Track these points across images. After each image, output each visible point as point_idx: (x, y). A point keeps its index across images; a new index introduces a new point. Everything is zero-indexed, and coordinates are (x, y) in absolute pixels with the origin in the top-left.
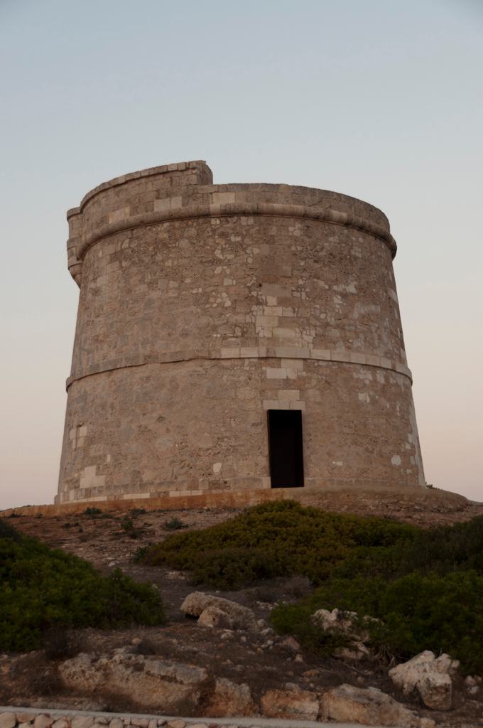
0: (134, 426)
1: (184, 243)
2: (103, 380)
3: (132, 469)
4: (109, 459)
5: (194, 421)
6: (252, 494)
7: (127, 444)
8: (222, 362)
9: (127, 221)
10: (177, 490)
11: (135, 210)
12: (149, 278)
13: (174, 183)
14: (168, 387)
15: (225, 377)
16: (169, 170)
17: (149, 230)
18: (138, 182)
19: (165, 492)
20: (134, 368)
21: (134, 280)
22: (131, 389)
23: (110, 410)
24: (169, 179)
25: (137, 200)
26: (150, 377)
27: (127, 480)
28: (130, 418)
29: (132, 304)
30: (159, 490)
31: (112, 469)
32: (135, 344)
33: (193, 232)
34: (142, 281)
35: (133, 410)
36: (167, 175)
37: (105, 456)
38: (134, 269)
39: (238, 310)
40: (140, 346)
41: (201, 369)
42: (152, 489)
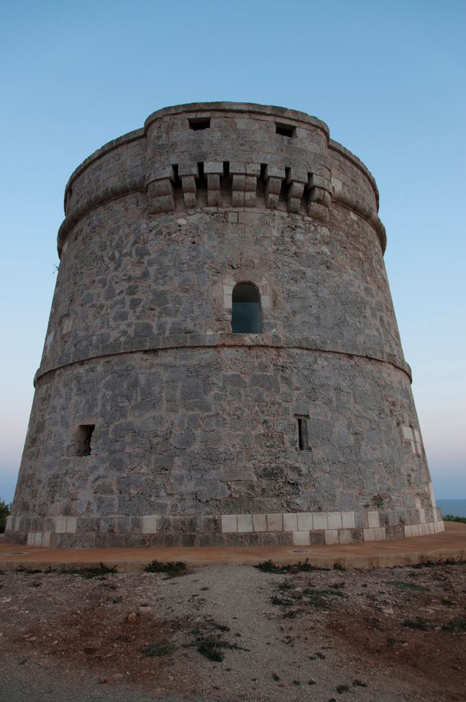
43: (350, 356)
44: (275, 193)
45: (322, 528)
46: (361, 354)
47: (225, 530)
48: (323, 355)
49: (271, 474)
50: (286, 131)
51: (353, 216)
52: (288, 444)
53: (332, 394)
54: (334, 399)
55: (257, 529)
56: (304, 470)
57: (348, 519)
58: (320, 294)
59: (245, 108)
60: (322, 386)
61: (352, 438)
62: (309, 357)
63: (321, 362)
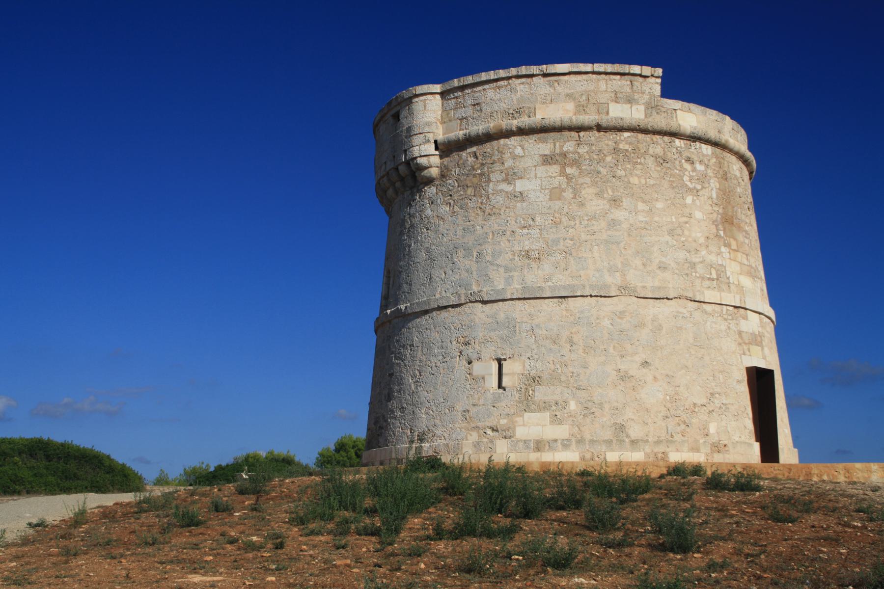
5: (684, 371)
8: (704, 305)
9: (571, 119)
10: (677, 450)
11: (581, 108)
13: (635, 88)
14: (651, 327)
15: (708, 323)
26: (624, 312)
27: (608, 434)
29: (588, 220)
30: (656, 450)
32: (598, 270)
39: (710, 248)
41: (684, 311)
42: (648, 449)
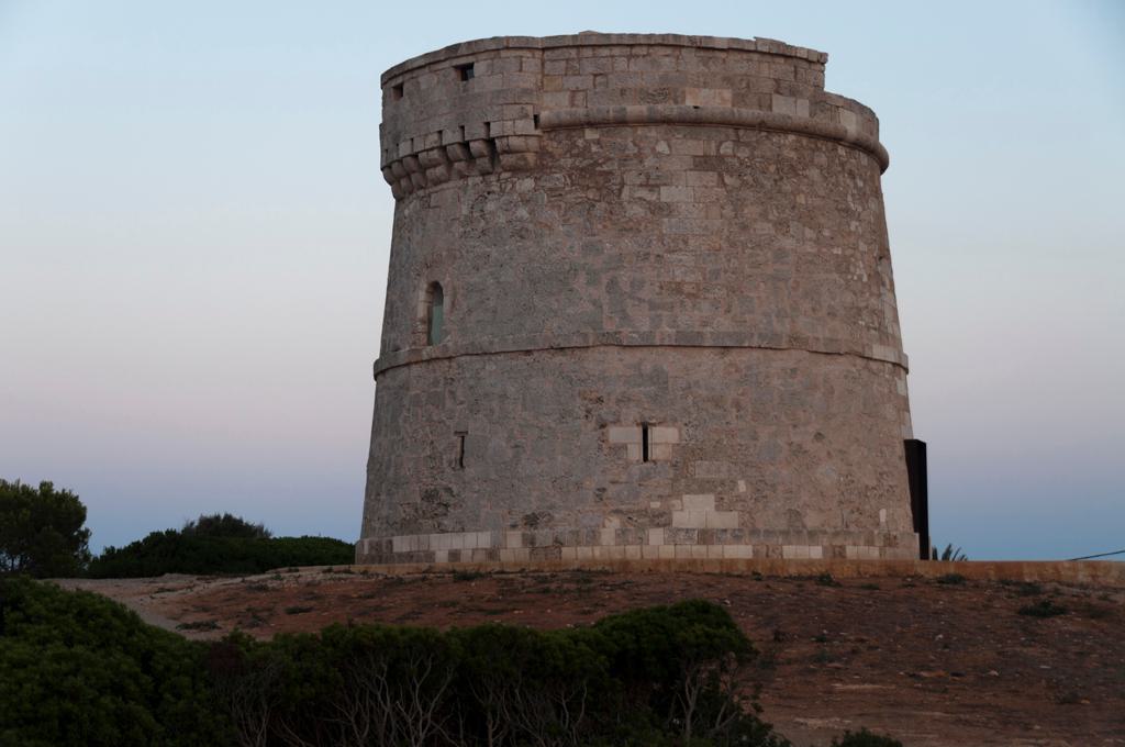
0: (781, 441)
1: (814, 173)
2: (707, 361)
3: (787, 508)
4: (742, 486)
6: (1081, 566)
7: (772, 468)
8: (871, 363)
11: (739, 99)
12: (774, 215)
13: (799, 76)
16: (798, 55)
17: (767, 137)
18: (745, 56)
19: (840, 547)
20: (770, 352)
21: (751, 211)
22: (768, 383)
23: (734, 410)
24: (793, 69)
25: (744, 85)
28: (774, 428)
31: (751, 503)
33: (822, 159)
34: (764, 216)
35: (776, 417)
36: (790, 61)
37: (734, 482)
38: (748, 194)
40: (773, 317)
43: (528, 352)
44: (460, 160)
45: (458, 547)
46: (541, 346)
47: (396, 550)
48: (493, 358)
49: (429, 496)
50: (465, 71)
51: (590, 134)
52: (445, 465)
53: (495, 404)
54: (497, 409)
55: (413, 549)
56: (455, 489)
57: (484, 540)
58: (502, 279)
59: (422, 62)
60: (486, 395)
61: (510, 453)
62: (477, 363)
63: (491, 367)
